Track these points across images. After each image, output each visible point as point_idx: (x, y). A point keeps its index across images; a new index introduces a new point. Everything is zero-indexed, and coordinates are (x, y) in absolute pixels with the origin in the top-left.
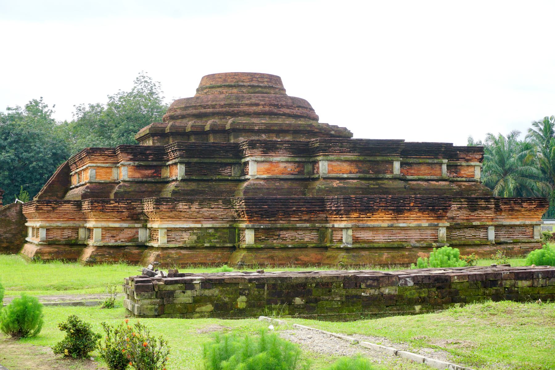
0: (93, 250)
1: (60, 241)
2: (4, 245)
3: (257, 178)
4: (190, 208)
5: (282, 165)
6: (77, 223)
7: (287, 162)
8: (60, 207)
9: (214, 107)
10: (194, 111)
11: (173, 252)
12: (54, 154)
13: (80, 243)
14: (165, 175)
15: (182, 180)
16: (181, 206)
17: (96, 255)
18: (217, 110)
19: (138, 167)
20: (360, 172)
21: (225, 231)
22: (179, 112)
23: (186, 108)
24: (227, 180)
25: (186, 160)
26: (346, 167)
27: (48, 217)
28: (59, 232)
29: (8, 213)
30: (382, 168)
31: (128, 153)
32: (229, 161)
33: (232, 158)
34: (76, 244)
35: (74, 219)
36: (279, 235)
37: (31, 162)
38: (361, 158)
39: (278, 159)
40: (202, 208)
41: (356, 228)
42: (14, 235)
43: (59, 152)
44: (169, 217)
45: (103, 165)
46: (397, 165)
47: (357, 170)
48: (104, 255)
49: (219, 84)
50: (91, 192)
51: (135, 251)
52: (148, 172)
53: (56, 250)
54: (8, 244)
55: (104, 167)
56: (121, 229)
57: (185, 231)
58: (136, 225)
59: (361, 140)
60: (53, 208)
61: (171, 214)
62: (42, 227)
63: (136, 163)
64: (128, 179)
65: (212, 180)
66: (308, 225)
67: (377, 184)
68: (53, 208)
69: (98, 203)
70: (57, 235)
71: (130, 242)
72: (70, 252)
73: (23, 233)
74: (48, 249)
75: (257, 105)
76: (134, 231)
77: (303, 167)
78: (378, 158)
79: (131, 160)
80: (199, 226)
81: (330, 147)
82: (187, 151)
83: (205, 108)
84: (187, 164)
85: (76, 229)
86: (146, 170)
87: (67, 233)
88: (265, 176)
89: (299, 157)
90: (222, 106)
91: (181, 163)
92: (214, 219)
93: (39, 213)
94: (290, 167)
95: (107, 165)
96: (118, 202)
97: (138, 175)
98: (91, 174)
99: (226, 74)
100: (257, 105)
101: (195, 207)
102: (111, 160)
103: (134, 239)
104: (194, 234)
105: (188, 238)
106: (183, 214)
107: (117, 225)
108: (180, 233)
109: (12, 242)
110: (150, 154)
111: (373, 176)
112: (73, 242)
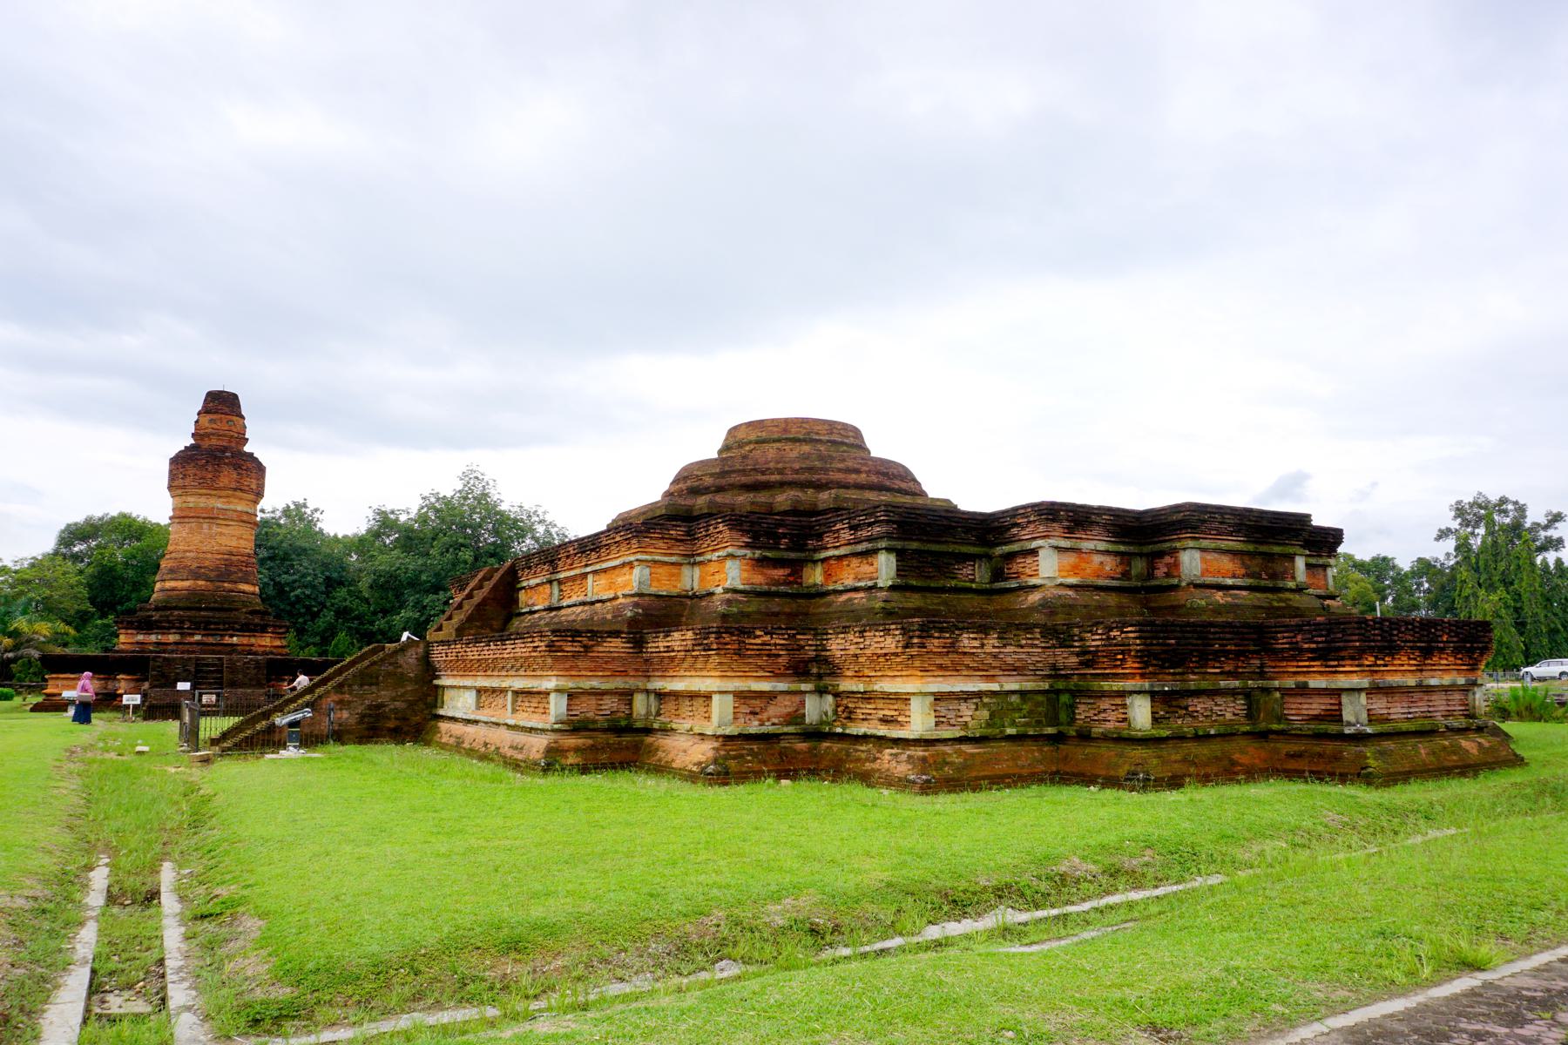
0: (716, 745)
1: (595, 722)
2: (391, 725)
3: (1061, 585)
4: (983, 645)
5: (1097, 559)
6: (631, 683)
7: (1107, 552)
8: (598, 644)
9: (781, 472)
10: (744, 479)
11: (947, 749)
12: (328, 579)
13: (639, 725)
14: (811, 581)
15: (892, 588)
16: (967, 641)
17: (726, 758)
18: (790, 477)
19: (761, 563)
20: (1248, 575)
21: (1040, 698)
22: (708, 481)
23: (723, 474)
24: (969, 590)
25: (899, 544)
26: (1226, 563)
27: (572, 668)
28: (593, 701)
29: (400, 659)
30: (1279, 568)
31: (745, 532)
32: (965, 549)
33: (974, 545)
34: (629, 729)
35: (624, 673)
36: (1186, 708)
37: (293, 589)
38: (1251, 547)
39: (1089, 545)
40: (1005, 646)
41: (1375, 690)
42: (411, 704)
43: (335, 575)
44: (941, 667)
45: (666, 559)
46: (1300, 563)
47: (1243, 571)
48: (742, 756)
49: (776, 436)
50: (646, 615)
51: (802, 746)
52: (779, 573)
53: (590, 742)
54: (397, 723)
55: (666, 563)
56: (770, 696)
57: (966, 700)
58: (804, 687)
59: (1250, 511)
60: (585, 646)
61: (945, 661)
62: (558, 691)
63: (758, 553)
64: (741, 587)
65: (943, 590)
66: (1237, 683)
67: (1281, 600)
68: (585, 646)
69: (732, 634)
70: (587, 708)
71: (789, 724)
72: (620, 748)
73: (430, 699)
74: (571, 741)
75: (858, 471)
76: (797, 699)
77: (1129, 564)
78: (1277, 549)
79: (747, 546)
80: (995, 687)
81: (1204, 521)
82: (900, 524)
83: (763, 473)
84: (901, 554)
85: (627, 695)
86: (775, 568)
87: (609, 704)
88: (1073, 580)
89: (1123, 543)
90: (797, 472)
91: (889, 550)
92: (1017, 670)
93: (556, 659)
94: (1110, 564)
95: (674, 559)
96: (771, 634)
97: (759, 579)
98: (641, 575)
99: (786, 420)
100: (858, 471)
101: (992, 641)
102: (681, 549)
103: (796, 717)
104: (985, 705)
105: (972, 718)
106: (967, 660)
107: (765, 686)
108: (954, 705)
109: (405, 719)
110: (784, 536)
111: (1269, 584)
112: (623, 723)
